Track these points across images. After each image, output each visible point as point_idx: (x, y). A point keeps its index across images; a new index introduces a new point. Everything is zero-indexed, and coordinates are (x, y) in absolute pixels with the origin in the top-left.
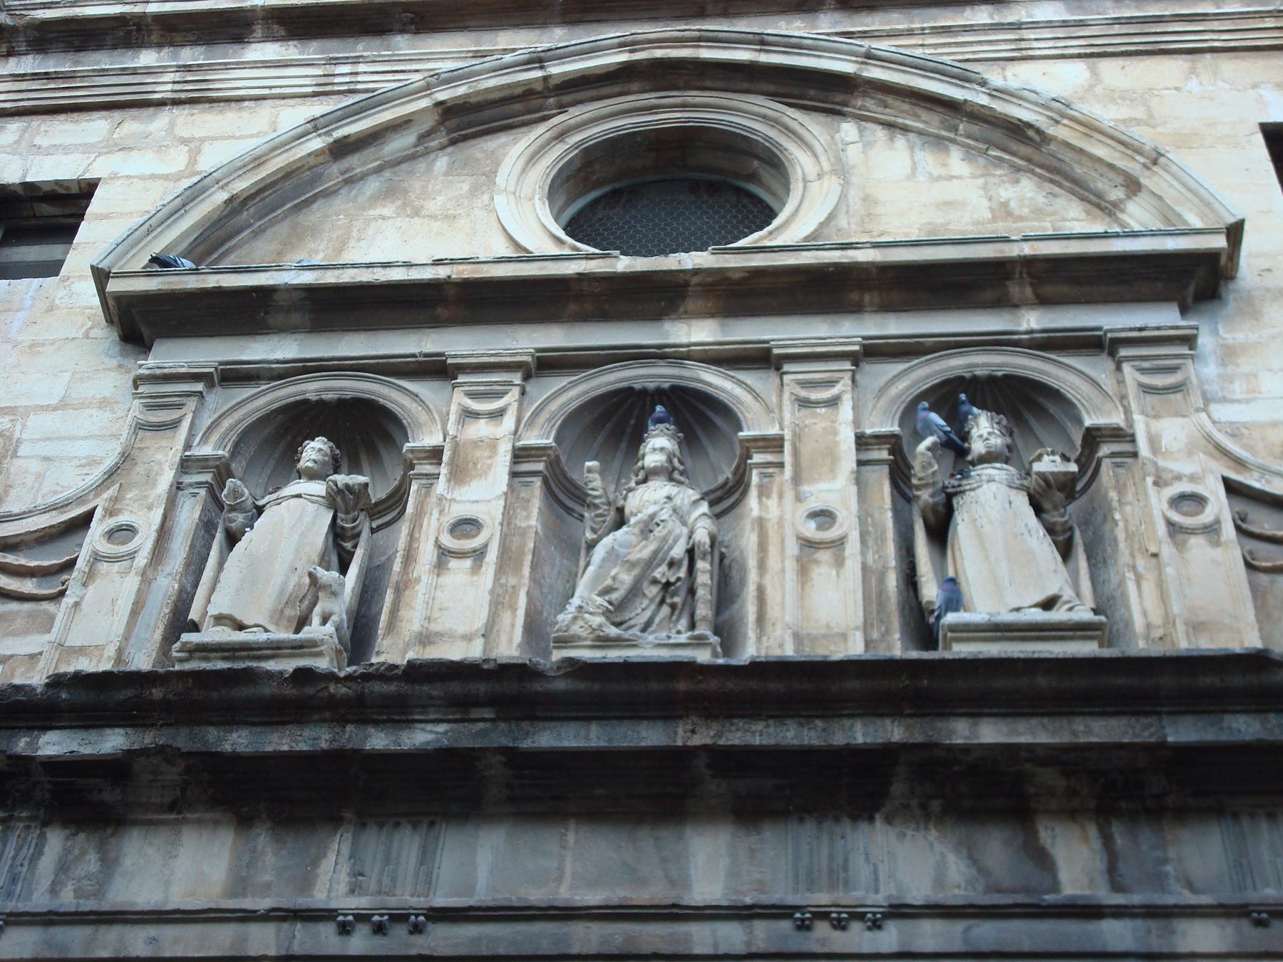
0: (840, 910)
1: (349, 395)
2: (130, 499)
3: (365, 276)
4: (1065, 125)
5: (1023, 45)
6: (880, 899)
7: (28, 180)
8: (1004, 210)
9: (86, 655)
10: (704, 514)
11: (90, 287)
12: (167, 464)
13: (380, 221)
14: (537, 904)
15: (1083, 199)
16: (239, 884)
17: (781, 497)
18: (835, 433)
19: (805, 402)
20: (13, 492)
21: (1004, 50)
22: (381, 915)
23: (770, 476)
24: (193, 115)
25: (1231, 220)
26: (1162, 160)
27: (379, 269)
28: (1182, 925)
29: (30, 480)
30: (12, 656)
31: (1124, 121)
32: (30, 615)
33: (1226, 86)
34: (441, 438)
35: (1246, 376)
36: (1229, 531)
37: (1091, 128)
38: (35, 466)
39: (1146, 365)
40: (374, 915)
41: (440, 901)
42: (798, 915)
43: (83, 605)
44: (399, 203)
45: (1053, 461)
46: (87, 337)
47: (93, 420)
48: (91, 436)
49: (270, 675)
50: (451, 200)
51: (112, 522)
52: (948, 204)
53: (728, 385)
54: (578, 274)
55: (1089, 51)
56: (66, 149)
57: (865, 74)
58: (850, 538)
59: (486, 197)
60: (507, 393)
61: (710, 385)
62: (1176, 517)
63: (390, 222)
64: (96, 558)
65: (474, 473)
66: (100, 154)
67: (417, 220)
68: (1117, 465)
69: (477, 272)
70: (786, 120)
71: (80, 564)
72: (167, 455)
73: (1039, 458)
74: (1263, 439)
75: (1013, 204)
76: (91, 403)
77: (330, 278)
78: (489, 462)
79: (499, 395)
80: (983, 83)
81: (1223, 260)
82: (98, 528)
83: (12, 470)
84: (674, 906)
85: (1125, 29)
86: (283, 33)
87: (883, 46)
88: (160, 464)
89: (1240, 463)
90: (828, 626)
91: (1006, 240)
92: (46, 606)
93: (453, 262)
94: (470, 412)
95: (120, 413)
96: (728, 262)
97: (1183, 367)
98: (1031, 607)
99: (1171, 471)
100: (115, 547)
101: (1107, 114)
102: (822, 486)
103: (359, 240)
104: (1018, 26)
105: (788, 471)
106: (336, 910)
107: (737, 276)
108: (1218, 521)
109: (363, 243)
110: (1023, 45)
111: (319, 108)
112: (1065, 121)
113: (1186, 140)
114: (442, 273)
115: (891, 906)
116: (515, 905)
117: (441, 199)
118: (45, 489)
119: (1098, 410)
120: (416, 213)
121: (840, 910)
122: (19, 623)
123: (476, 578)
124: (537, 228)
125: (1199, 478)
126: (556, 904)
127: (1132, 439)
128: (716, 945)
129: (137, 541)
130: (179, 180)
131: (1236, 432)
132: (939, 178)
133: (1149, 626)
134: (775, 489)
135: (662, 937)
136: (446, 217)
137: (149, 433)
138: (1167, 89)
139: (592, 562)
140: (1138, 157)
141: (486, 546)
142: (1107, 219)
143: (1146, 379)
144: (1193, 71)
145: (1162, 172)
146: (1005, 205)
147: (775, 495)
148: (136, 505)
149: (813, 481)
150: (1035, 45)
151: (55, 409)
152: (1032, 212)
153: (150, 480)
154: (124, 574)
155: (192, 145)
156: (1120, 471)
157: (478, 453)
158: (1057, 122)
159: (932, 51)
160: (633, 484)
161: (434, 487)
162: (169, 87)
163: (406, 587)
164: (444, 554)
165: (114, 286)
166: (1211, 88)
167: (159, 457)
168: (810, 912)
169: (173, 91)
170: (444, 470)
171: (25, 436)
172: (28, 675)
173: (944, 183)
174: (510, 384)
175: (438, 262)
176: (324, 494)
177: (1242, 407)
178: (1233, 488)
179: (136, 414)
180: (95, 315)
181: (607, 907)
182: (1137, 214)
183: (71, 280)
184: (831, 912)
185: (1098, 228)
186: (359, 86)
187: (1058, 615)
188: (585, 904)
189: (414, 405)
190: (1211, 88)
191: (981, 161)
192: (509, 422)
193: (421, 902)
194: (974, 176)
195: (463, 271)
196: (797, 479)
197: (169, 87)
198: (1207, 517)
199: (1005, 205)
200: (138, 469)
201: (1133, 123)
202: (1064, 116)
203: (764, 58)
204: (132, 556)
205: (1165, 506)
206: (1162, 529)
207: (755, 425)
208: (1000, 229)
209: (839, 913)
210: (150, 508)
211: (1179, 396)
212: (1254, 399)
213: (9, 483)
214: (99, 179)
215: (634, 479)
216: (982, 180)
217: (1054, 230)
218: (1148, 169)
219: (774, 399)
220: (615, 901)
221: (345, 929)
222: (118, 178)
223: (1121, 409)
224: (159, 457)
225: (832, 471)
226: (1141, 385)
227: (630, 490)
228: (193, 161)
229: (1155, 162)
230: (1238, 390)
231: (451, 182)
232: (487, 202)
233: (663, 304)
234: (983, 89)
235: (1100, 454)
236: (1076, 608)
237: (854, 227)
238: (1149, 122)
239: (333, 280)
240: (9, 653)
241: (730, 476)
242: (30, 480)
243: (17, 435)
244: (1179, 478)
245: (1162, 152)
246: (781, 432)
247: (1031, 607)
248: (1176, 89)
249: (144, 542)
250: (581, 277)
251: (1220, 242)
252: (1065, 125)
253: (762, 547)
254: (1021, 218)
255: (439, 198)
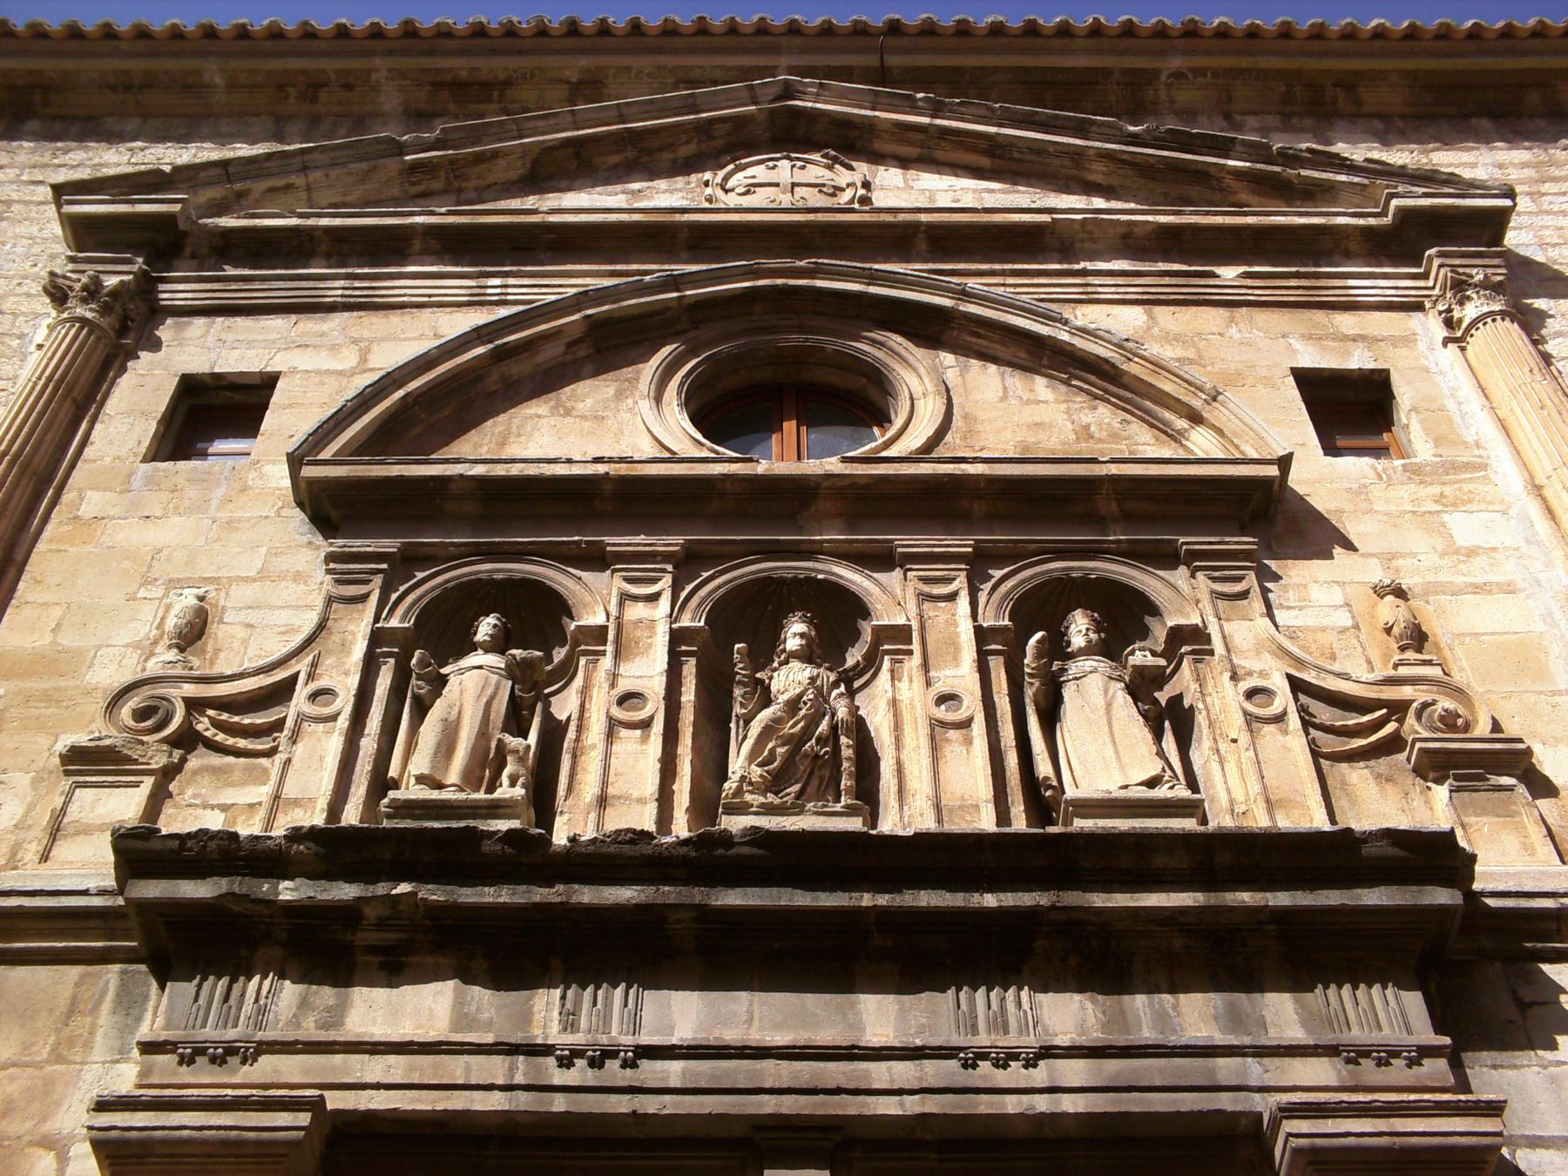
0: (998, 1050)
1: (519, 576)
2: (328, 665)
3: (532, 470)
4: (1137, 363)
5: (1090, 289)
6: (1031, 1041)
7: (217, 370)
8: (1085, 432)
9: (300, 806)
10: (842, 694)
11: (284, 469)
12: (361, 634)
13: (536, 419)
14: (732, 1044)
15: (1152, 426)
16: (461, 1018)
17: (911, 681)
18: (956, 626)
19: (927, 596)
20: (222, 655)
21: (1074, 293)
22: (594, 1051)
23: (901, 661)
24: (361, 317)
25: (1282, 453)
26: (1220, 398)
27: (545, 465)
28: (1095, 1035)
29: (236, 644)
30: (233, 805)
31: (1178, 360)
32: (246, 768)
33: (1261, 334)
34: (605, 619)
35: (1298, 586)
36: (1294, 721)
37: (1157, 365)
38: (241, 633)
39: (1217, 574)
40: (588, 1050)
41: (646, 1039)
42: (962, 1055)
43: (294, 761)
44: (552, 403)
45: (1145, 656)
46: (279, 516)
47: (290, 592)
48: (288, 606)
49: (490, 835)
50: (598, 402)
51: (313, 686)
52: (1039, 425)
53: (866, 583)
54: (723, 475)
55: (1145, 297)
56: (250, 345)
57: (961, 308)
58: (976, 719)
59: (630, 401)
60: (660, 580)
61: (841, 577)
62: (1250, 708)
63: (545, 421)
64: (301, 718)
65: (636, 651)
66: (279, 350)
67: (569, 420)
68: (1197, 661)
69: (632, 470)
70: (891, 343)
71: (289, 723)
72: (359, 626)
73: (1132, 653)
74: (1315, 642)
75: (1093, 428)
76: (286, 576)
77: (500, 470)
78: (649, 641)
79: (655, 581)
80: (1066, 322)
81: (1276, 486)
82: (301, 692)
83: (220, 635)
84: (853, 1047)
85: (1174, 281)
86: (438, 247)
87: (972, 283)
88: (353, 634)
89: (1300, 663)
90: (963, 798)
91: (1094, 461)
92: (264, 761)
93: (611, 460)
94: (629, 596)
95: (313, 587)
96: (857, 470)
97: (1247, 578)
98: (1137, 785)
99: (1244, 668)
100: (320, 709)
101: (1167, 353)
102: (948, 672)
103: (519, 435)
104: (1084, 273)
105: (916, 659)
106: (554, 1045)
107: (863, 481)
108: (1284, 713)
109: (522, 439)
110: (1090, 289)
111: (479, 317)
112: (1136, 359)
113: (1236, 378)
114: (601, 469)
115: (1041, 1048)
116: (712, 1043)
117: (589, 402)
118: (251, 652)
119: (1181, 612)
120: (568, 413)
121: (998, 1050)
122: (237, 775)
123: (644, 747)
124: (681, 435)
125: (1267, 674)
126: (749, 1044)
127: (1208, 640)
128: (892, 1081)
129: (338, 703)
130: (352, 375)
131: (1294, 635)
132: (1028, 402)
133: (1232, 802)
134: (905, 673)
135: (844, 1073)
136: (596, 417)
137: (341, 606)
138: (1214, 334)
139: (749, 735)
140: (1200, 394)
141: (652, 718)
142: (1174, 444)
143: (1219, 587)
144: (1232, 320)
145: (1221, 408)
146: (1087, 427)
147: (905, 678)
148: (334, 671)
149: (940, 668)
150: (1100, 289)
151: (255, 580)
152: (1109, 436)
153: (345, 648)
154: (329, 733)
155: (361, 344)
156: (1199, 665)
157: (639, 633)
158: (1130, 360)
159: (1012, 290)
160: (775, 664)
161: (599, 663)
162: (339, 292)
163: (582, 754)
164: (613, 726)
165: (308, 472)
166: (1248, 335)
167: (351, 627)
168: (973, 1053)
169: (342, 296)
170: (610, 648)
171: (229, 604)
172: (249, 822)
173: (1033, 406)
174: (664, 571)
175: (597, 460)
176: (503, 666)
177: (1295, 612)
178: (1297, 685)
179: (329, 587)
180: (285, 496)
181: (794, 1047)
182: (1202, 442)
183: (261, 463)
184: (991, 1053)
185: (1167, 453)
186: (509, 297)
187: (1162, 792)
188: (775, 1044)
189: (578, 587)
190: (1248, 335)
191: (1063, 388)
192: (664, 604)
193: (628, 1040)
194: (1057, 401)
195: (620, 468)
196: (925, 666)
197: (339, 292)
198: (1276, 708)
199: (1087, 427)
200: (333, 638)
201: (1187, 362)
202: (1136, 355)
203: (873, 290)
204: (333, 718)
205: (1242, 698)
206: (1239, 720)
207: (886, 613)
208: (1084, 450)
209: (997, 1053)
210: (346, 673)
211: (1245, 602)
212: (1305, 607)
213: (218, 647)
214: (280, 372)
215: (777, 660)
216: (1065, 406)
217: (1130, 453)
218: (1208, 404)
219: (899, 591)
220: (802, 1043)
221: (969, 1065)
222: (298, 373)
223: (1197, 611)
224: (351, 627)
225: (955, 659)
226: (1213, 592)
227: (775, 670)
228: (363, 359)
229: (1214, 399)
230: (1292, 599)
231: (598, 386)
232: (631, 406)
233: (797, 503)
234: (1065, 328)
235: (1182, 650)
236: (1176, 787)
237: (958, 441)
238: (1198, 361)
239: (503, 473)
240: (230, 802)
241: (860, 659)
242: (236, 644)
243: (222, 602)
244: (1250, 674)
245: (1221, 391)
246: (908, 623)
247: (1137, 785)
248: (1219, 334)
249: (344, 703)
250: (726, 477)
251: (1273, 471)
252: (1137, 363)
253: (897, 727)
254: (1100, 440)
255: (588, 401)
